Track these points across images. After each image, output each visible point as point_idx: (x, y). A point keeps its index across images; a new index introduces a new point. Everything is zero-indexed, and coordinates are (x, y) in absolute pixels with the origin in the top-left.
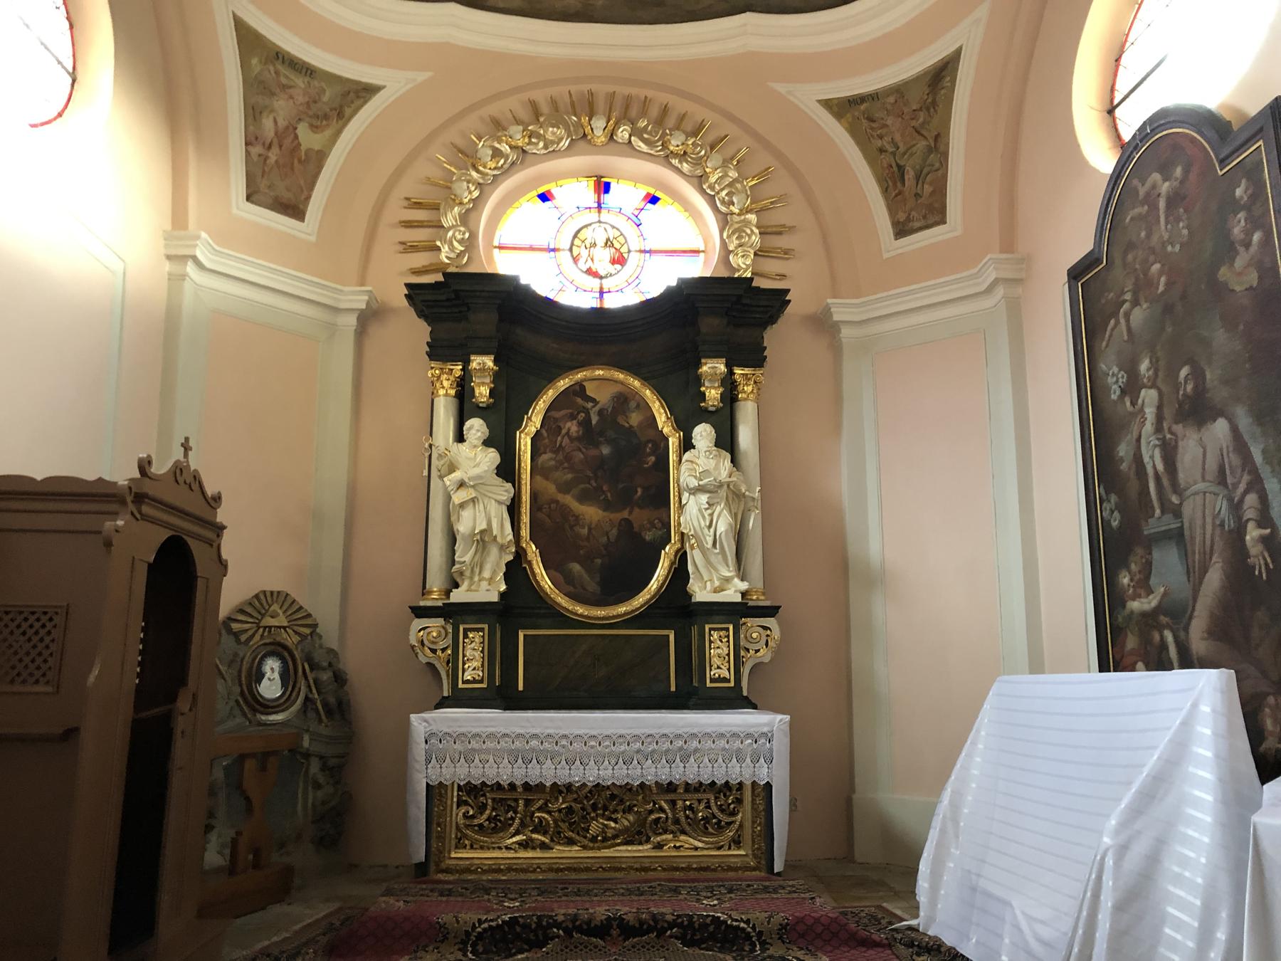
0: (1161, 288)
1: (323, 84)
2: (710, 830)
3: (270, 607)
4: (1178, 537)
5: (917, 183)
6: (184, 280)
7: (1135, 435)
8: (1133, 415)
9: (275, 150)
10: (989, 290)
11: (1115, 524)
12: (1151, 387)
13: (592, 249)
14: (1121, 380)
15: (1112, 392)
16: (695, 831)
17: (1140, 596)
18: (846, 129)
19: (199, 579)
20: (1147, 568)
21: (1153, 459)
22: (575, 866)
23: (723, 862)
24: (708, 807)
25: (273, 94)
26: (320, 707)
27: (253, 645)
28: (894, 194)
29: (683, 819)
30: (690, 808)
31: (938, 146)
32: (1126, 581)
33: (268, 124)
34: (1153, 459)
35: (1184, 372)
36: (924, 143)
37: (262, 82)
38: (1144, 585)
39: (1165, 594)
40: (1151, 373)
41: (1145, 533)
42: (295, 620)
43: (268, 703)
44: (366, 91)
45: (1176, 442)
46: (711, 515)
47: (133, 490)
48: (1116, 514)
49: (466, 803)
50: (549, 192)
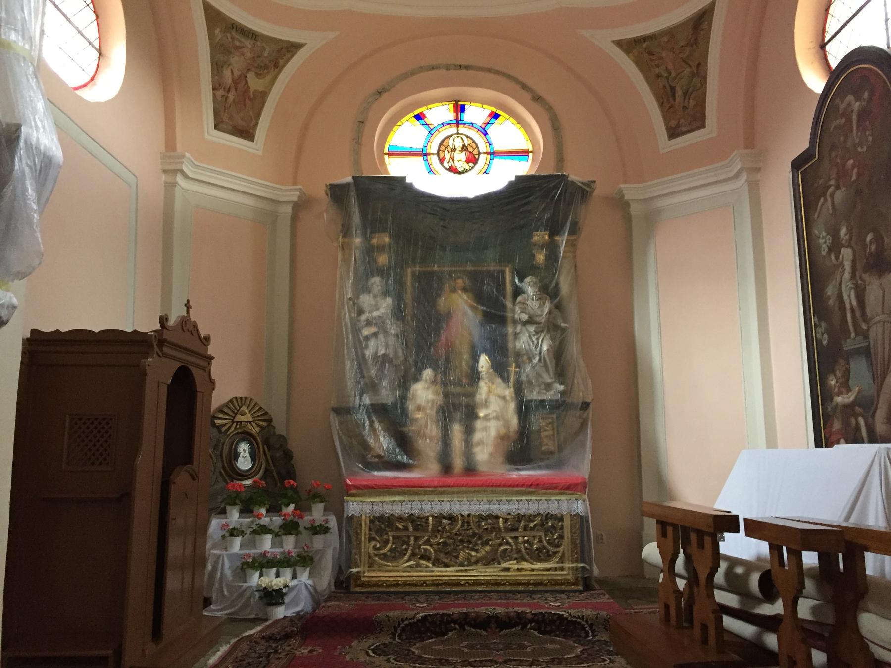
0: (854, 178)
1: (264, 44)
2: (542, 557)
3: (240, 408)
4: (867, 352)
5: (684, 100)
6: (175, 186)
7: (838, 280)
8: (836, 267)
9: (233, 92)
10: (737, 176)
11: (825, 343)
12: (847, 247)
13: (453, 153)
14: (828, 241)
15: (822, 249)
16: (531, 558)
17: (842, 394)
18: (633, 61)
19: (198, 393)
20: (847, 374)
21: (850, 298)
22: (450, 582)
23: (553, 580)
24: (540, 541)
25: (230, 53)
26: (276, 477)
27: (230, 434)
28: (667, 108)
29: (523, 549)
30: (527, 542)
31: (700, 73)
32: (833, 383)
33: (227, 73)
34: (850, 298)
35: (869, 237)
36: (688, 70)
37: (222, 45)
38: (845, 386)
39: (859, 392)
40: (847, 237)
41: (845, 349)
42: (257, 417)
43: (243, 473)
44: (293, 48)
45: (865, 285)
46: (537, 339)
47: (157, 338)
48: (825, 336)
49: (374, 539)
50: (422, 113)
